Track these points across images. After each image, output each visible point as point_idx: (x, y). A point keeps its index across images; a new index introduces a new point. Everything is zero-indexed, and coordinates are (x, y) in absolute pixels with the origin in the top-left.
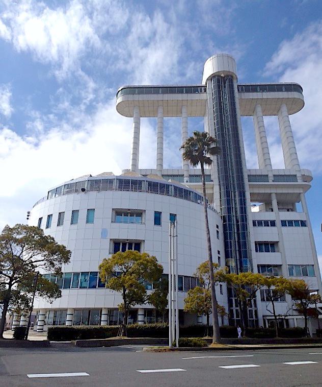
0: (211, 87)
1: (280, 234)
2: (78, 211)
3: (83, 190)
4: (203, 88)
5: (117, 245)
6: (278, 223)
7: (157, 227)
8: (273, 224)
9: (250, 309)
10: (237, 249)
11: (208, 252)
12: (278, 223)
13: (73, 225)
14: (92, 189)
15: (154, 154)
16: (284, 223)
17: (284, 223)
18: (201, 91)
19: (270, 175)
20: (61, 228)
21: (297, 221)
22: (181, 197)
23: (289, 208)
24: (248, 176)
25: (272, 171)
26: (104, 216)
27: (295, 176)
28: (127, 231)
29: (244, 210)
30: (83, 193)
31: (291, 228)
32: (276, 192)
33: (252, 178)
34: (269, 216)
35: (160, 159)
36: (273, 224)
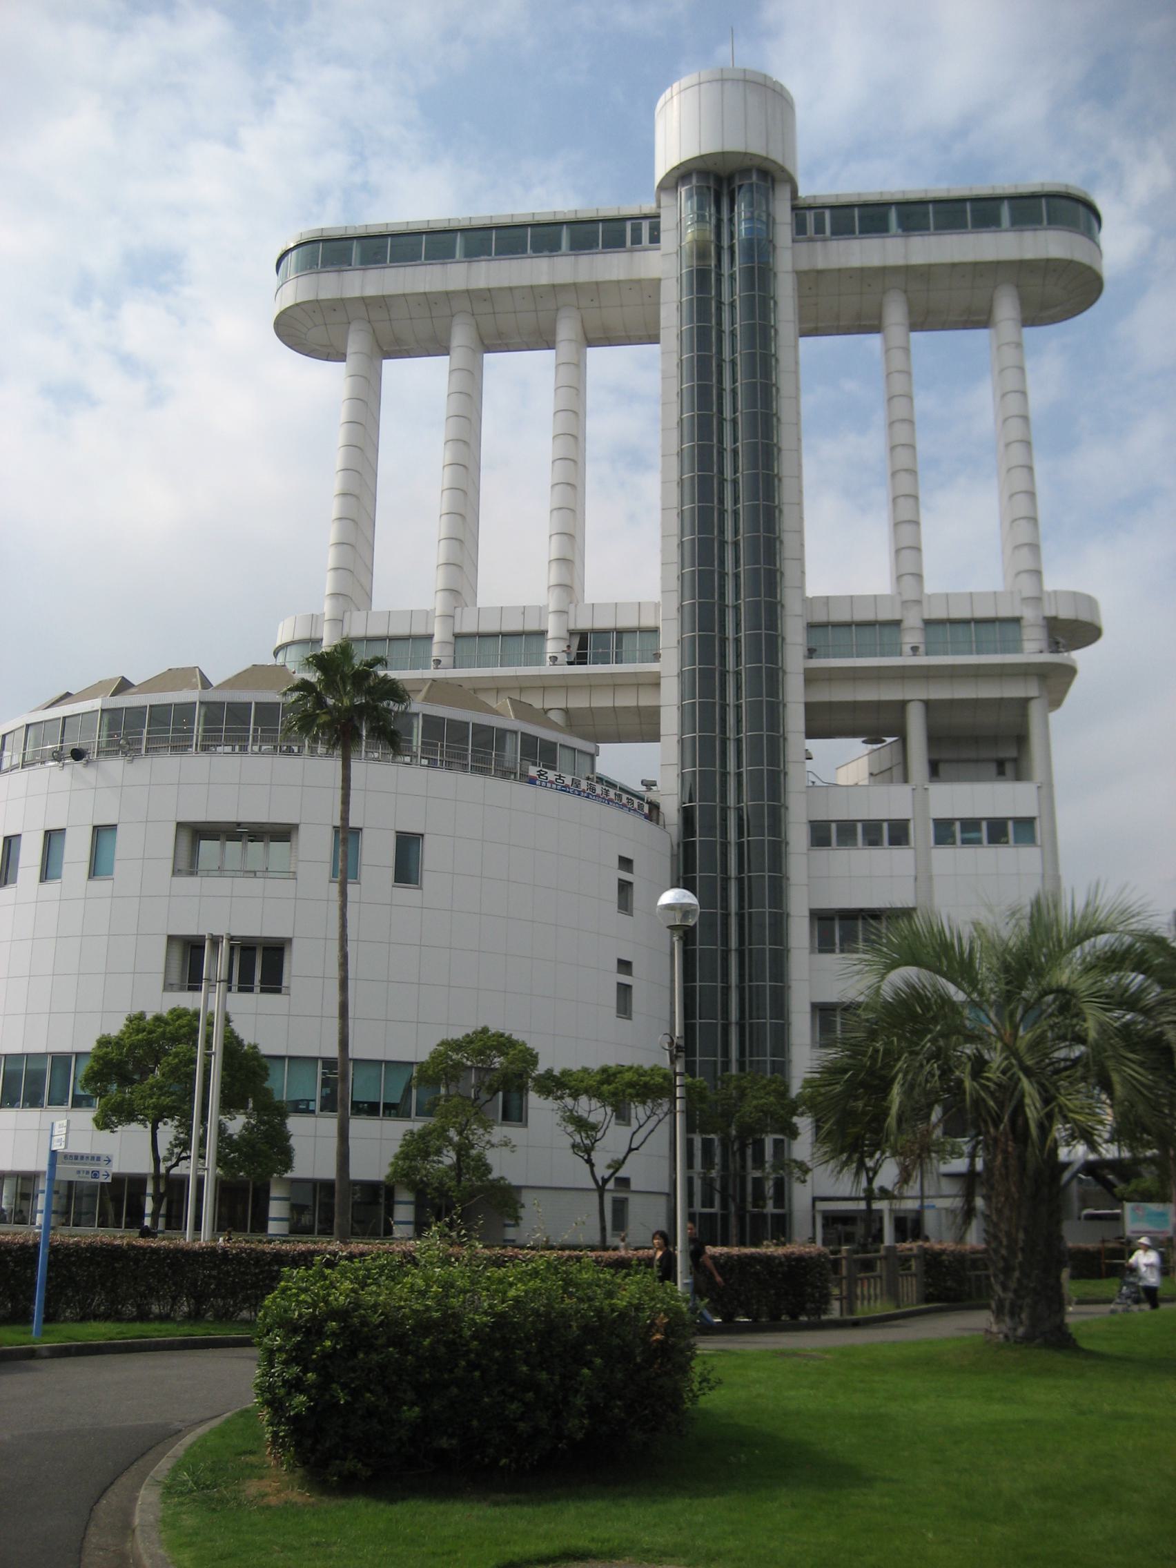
0: (681, 220)
1: (924, 878)
2: (19, 835)
3: (78, 755)
4: (645, 226)
5: (189, 955)
6: (921, 833)
7: (406, 894)
8: (899, 833)
9: (758, 1174)
10: (734, 944)
11: (335, 1024)
12: (921, 833)
13: (47, 887)
14: (112, 748)
15: (541, 546)
16: (944, 831)
17: (944, 831)
18: (637, 240)
19: (913, 620)
20: (52, 887)
21: (971, 825)
22: (455, 761)
23: (1003, 754)
24: (812, 626)
25: (918, 602)
26: (146, 847)
27: (1017, 621)
28: (230, 905)
29: (773, 783)
30: (79, 765)
31: (969, 852)
32: (924, 697)
33: (828, 630)
34: (893, 802)
35: (569, 562)
36: (899, 833)
